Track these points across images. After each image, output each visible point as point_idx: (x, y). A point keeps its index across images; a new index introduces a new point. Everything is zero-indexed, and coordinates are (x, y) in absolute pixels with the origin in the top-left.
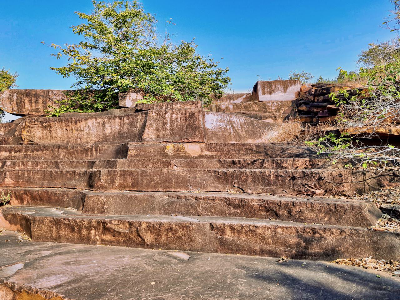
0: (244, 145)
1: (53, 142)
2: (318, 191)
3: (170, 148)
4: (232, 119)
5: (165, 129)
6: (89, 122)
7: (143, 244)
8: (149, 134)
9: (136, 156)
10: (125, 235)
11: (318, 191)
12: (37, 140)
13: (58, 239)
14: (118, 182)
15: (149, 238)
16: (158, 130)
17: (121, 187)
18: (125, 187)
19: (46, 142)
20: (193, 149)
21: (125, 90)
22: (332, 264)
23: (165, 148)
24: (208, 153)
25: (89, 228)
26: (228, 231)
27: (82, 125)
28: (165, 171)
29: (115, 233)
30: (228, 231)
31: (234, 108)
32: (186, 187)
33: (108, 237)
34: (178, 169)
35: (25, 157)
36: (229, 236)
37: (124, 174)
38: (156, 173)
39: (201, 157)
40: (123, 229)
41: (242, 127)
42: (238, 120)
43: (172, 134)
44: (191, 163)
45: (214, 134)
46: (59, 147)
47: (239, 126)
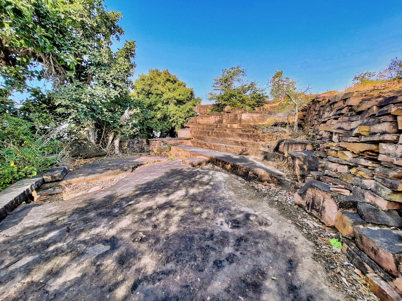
0: (250, 125)
1: (204, 123)
2: (258, 140)
3: (229, 126)
4: (253, 115)
5: (228, 119)
6: (212, 117)
7: (212, 149)
8: (224, 121)
9: (219, 128)
10: (209, 147)
11: (258, 140)
12: (200, 122)
13: (198, 147)
14: (213, 135)
15: (213, 148)
16: (226, 120)
17: (214, 136)
18: (215, 136)
19: (202, 123)
20: (235, 126)
21: (225, 105)
22: (127, 212)
23: (227, 125)
24: (240, 127)
25: (203, 145)
26: (228, 148)
27: (210, 117)
28: (225, 132)
29: (208, 146)
30: (228, 148)
31: (270, 108)
32: (229, 137)
33: (206, 147)
34: (228, 132)
35: (197, 127)
36: (228, 149)
37: (215, 132)
38: (222, 133)
39: (237, 128)
40: (209, 145)
41: (257, 118)
42: (256, 116)
43: (230, 121)
44: (233, 130)
45: (245, 121)
46: (204, 124)
47: (256, 118)
